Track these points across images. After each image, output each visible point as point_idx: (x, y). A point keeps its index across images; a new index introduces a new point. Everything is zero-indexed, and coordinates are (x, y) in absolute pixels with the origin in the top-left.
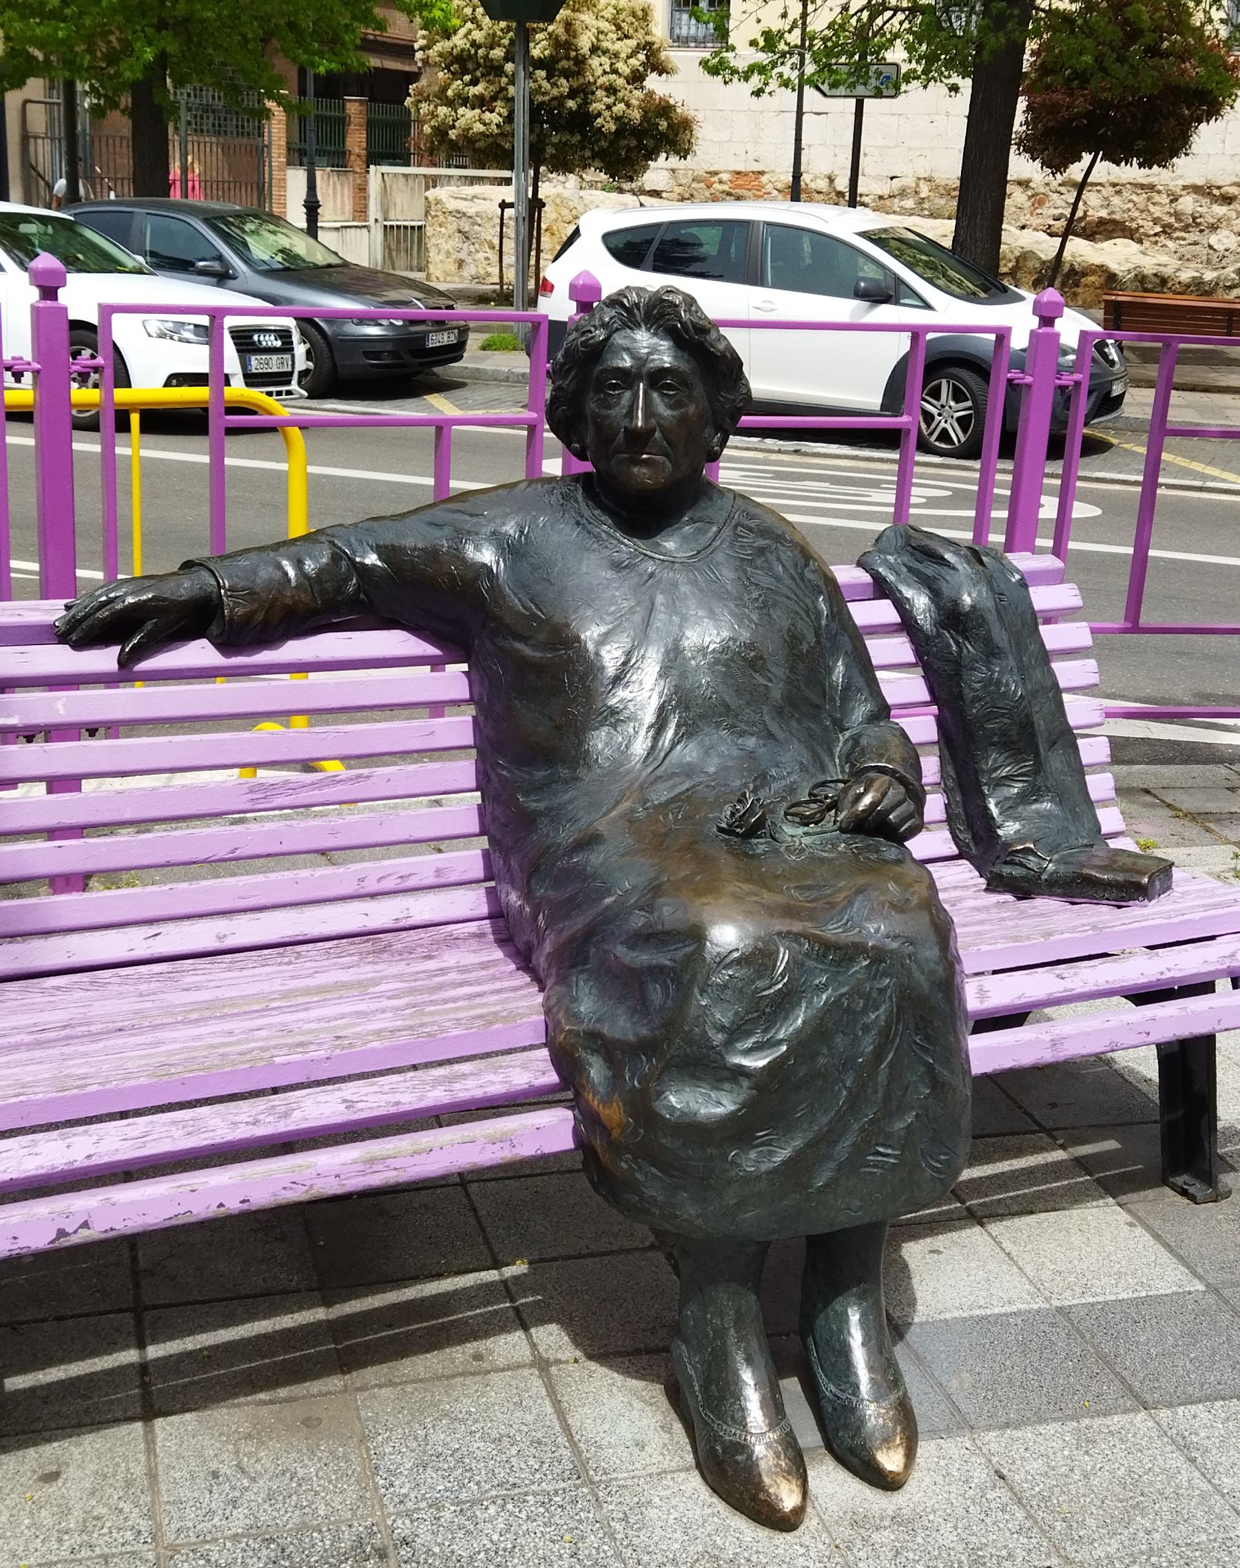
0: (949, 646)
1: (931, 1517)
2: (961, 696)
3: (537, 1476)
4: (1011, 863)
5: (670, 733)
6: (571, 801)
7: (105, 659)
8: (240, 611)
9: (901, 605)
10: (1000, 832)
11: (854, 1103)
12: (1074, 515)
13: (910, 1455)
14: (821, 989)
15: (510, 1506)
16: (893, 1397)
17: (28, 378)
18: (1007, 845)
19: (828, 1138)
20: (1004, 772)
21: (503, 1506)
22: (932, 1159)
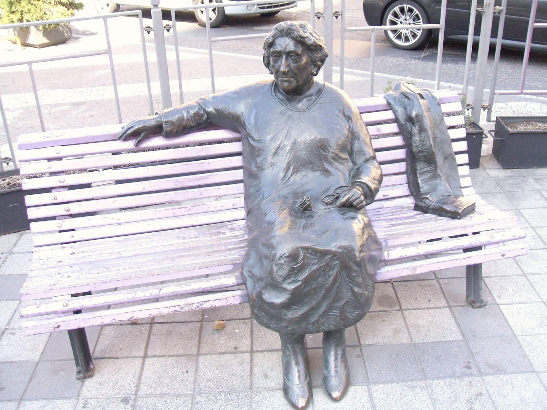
0: (408, 128)
2: (411, 144)
4: (421, 201)
5: (291, 171)
7: (130, 144)
8: (169, 129)
9: (395, 112)
10: (421, 190)
11: (324, 297)
17: (152, 32)
18: (422, 194)
19: (319, 305)
20: (426, 169)
21: (226, 396)
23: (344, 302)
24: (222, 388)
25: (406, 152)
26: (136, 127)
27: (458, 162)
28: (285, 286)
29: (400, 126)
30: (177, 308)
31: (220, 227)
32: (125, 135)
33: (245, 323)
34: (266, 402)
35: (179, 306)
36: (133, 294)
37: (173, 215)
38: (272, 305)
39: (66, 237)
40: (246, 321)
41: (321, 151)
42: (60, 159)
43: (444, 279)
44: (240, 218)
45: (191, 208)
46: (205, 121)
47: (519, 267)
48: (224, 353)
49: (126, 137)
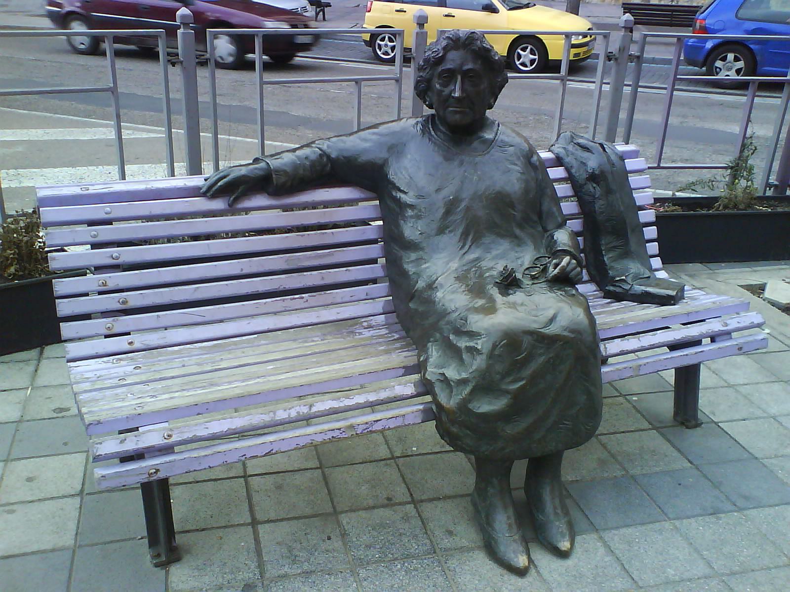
1: (582, 569)
3: (417, 551)
6: (427, 268)
7: (218, 204)
12: (624, 129)
13: (572, 544)
14: (541, 355)
15: (406, 564)
16: (566, 519)
22: (586, 425)
23: (579, 407)
24: (392, 554)
25: (584, 221)
26: (232, 176)
27: (647, 237)
28: (504, 387)
29: (574, 187)
30: (336, 434)
31: (352, 326)
32: (214, 189)
33: (387, 465)
34: (467, 568)
35: (339, 429)
36: (272, 414)
37: (283, 309)
38: (484, 416)
39: (120, 343)
40: (388, 462)
41: (510, 209)
42: (108, 222)
43: (631, 395)
44: (376, 311)
45: (309, 298)
46: (331, 171)
47: (720, 377)
48: (374, 508)
49: (212, 192)
